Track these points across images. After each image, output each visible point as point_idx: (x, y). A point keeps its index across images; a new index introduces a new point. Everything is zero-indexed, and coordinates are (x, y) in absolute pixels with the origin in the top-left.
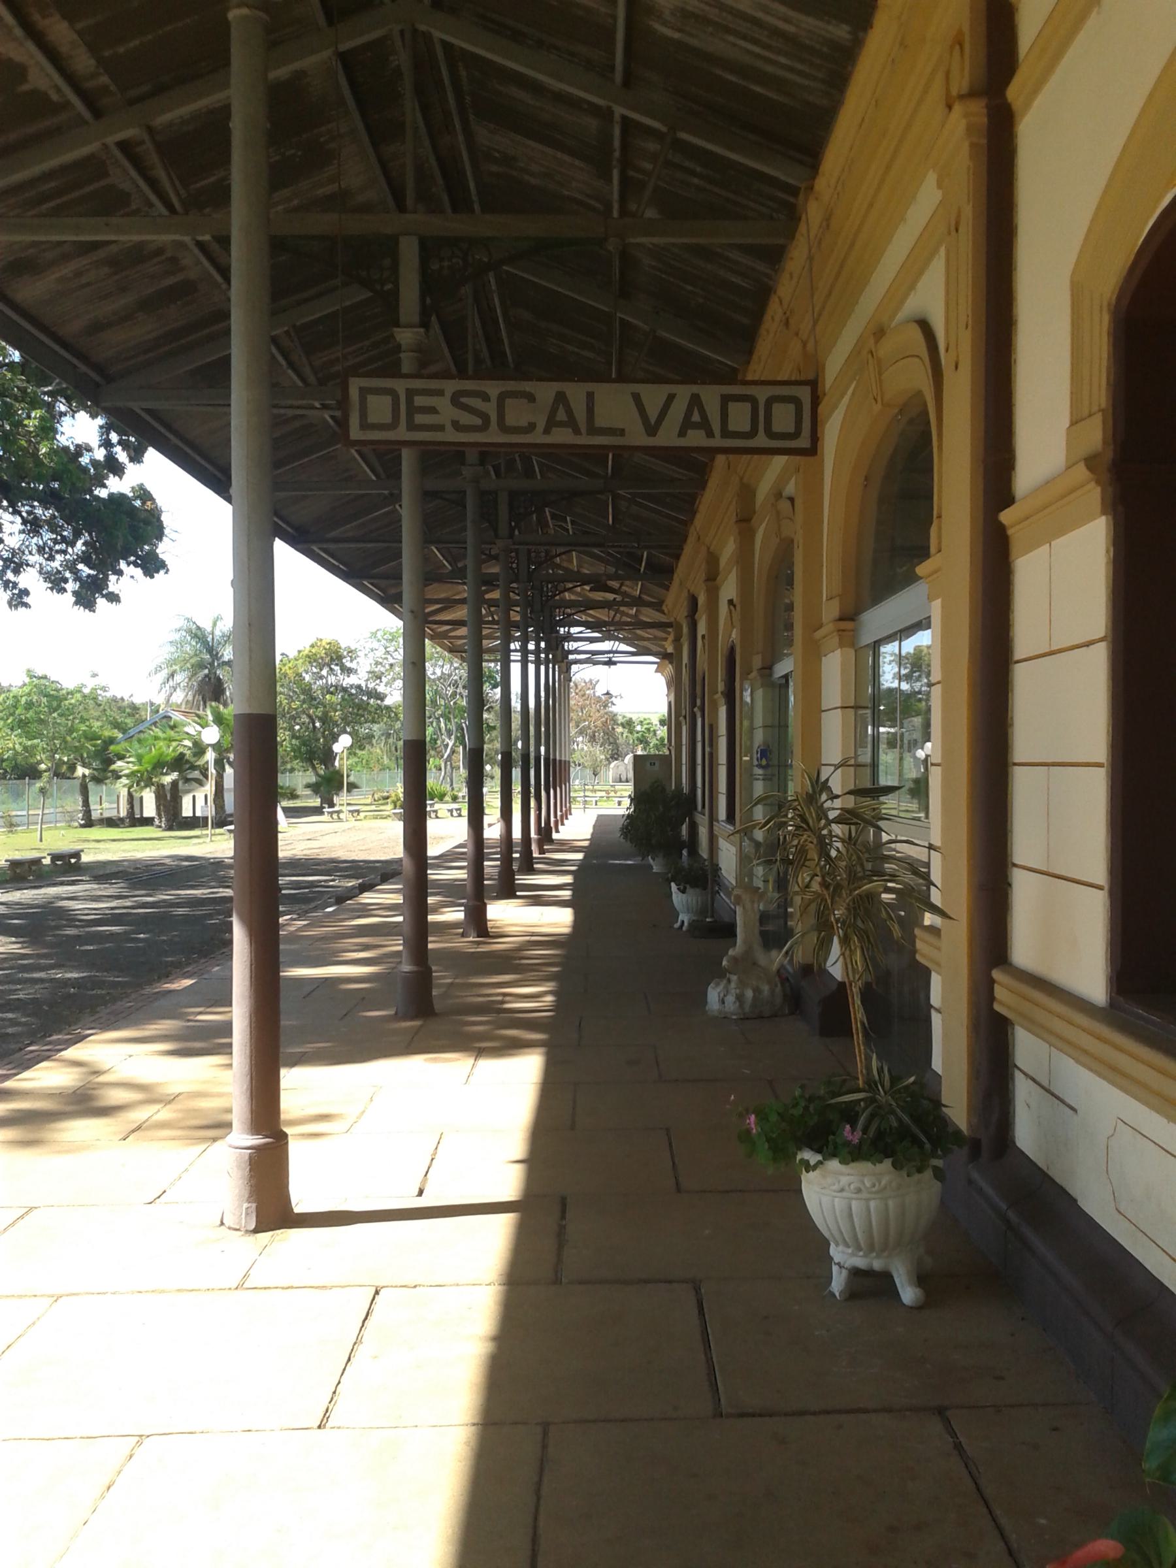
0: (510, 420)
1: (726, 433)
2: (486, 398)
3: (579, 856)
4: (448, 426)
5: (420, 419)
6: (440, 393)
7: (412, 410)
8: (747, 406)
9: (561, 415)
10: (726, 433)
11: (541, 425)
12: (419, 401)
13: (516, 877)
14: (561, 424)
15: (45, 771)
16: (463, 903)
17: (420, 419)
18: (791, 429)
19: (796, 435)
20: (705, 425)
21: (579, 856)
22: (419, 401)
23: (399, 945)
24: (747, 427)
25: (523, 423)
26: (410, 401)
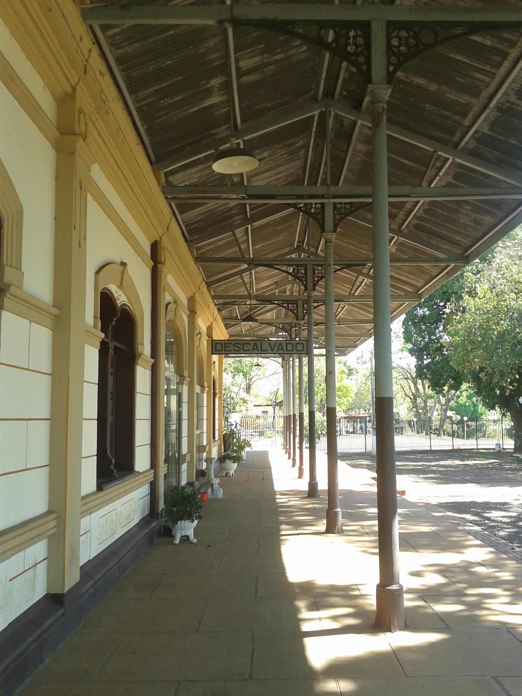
0: (245, 349)
1: (262, 350)
2: (240, 345)
3: (373, 330)
4: (233, 350)
5: (226, 349)
6: (231, 343)
7: (225, 347)
8: (291, 345)
9: (280, 347)
10: (287, 350)
11: (251, 350)
12: (227, 345)
13: (397, 463)
14: (255, 349)
15: (500, 247)
16: (331, 61)
17: (226, 349)
18: (298, 349)
19: (303, 350)
20: (282, 349)
21: (373, 330)
22: (227, 345)
23: (398, 465)
24: (220, 349)
25: (248, 349)
26: (225, 346)
